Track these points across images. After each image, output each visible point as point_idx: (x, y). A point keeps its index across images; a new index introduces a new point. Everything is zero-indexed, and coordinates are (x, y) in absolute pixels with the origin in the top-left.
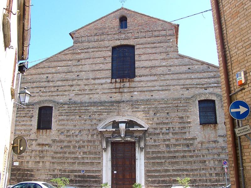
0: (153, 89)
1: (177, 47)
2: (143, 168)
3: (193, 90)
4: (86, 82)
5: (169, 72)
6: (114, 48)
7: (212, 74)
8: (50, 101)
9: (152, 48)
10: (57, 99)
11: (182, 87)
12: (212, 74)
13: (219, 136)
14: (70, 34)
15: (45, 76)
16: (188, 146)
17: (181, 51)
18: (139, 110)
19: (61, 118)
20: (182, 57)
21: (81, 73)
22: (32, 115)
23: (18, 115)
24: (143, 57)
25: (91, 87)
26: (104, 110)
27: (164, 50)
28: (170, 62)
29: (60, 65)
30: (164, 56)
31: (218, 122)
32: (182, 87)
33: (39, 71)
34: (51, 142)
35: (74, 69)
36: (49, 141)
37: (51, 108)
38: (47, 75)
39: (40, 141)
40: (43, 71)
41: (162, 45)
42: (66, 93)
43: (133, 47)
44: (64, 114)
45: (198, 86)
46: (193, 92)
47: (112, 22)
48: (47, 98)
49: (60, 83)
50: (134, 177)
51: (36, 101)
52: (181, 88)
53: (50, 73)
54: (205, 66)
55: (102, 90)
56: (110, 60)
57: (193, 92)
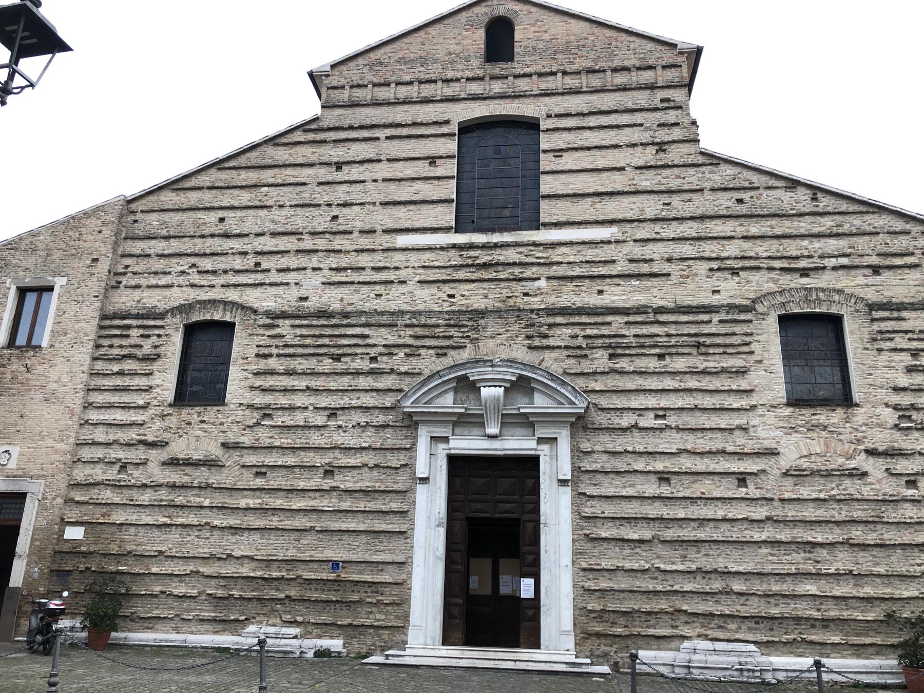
0: (603, 270)
1: (694, 127)
2: (566, 558)
3: (755, 277)
4: (365, 242)
5: (664, 214)
6: (467, 129)
7: (827, 223)
8: (227, 304)
9: (264, 390)
10: (251, 297)
11: (715, 265)
12: (827, 223)
13: (871, 452)
14: (311, 75)
15: (213, 217)
16: (742, 479)
17: (709, 141)
18: (552, 342)
19: (262, 364)
20: (714, 160)
21: (346, 211)
22: (154, 351)
23: (102, 351)
24: (569, 161)
25: (379, 260)
26: (427, 342)
27: (646, 137)
28: (671, 179)
29: (271, 181)
30: (648, 156)
31: (856, 397)
32: (715, 265)
33: (193, 198)
34: (216, 451)
35: (323, 195)
36: (212, 449)
37: (230, 327)
38: (221, 214)
39: (179, 448)
40: (207, 198)
41: (638, 118)
42: (291, 277)
43: (531, 126)
44: (275, 351)
45: (777, 264)
46: (761, 282)
47: (460, 37)
48: (217, 294)
49: (269, 244)
50: (458, 481)
51: (176, 304)
52: (711, 270)
53: (232, 208)
54: (803, 195)
55: (420, 271)
56: (450, 168)
57: (761, 282)
